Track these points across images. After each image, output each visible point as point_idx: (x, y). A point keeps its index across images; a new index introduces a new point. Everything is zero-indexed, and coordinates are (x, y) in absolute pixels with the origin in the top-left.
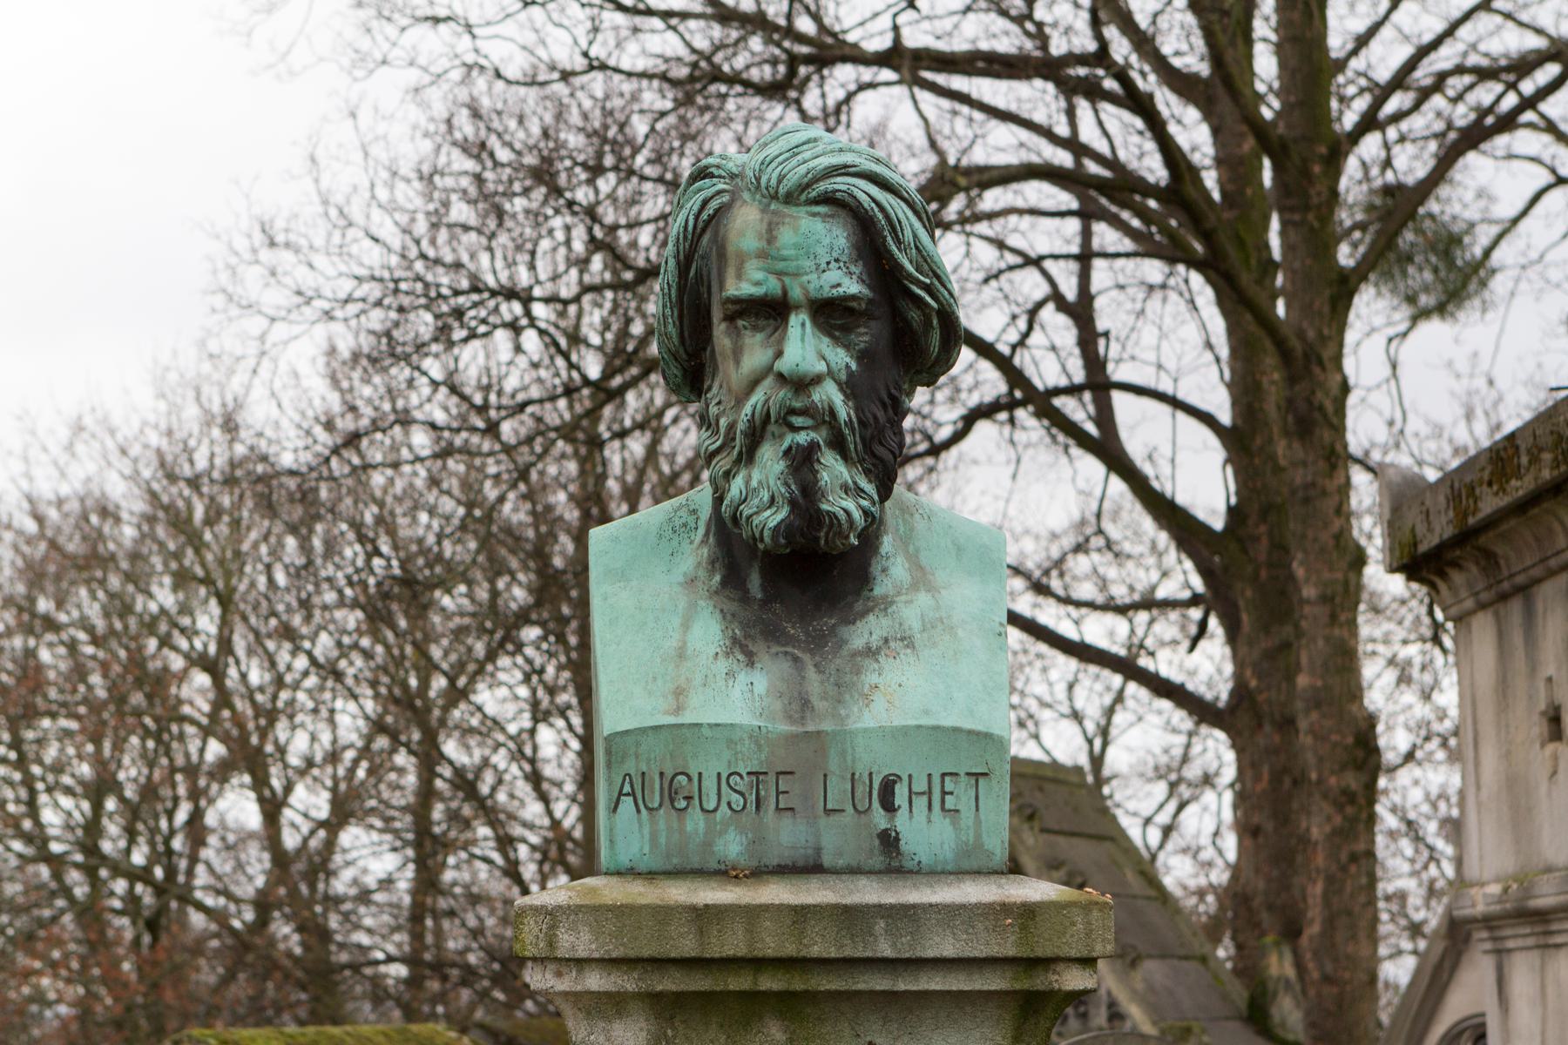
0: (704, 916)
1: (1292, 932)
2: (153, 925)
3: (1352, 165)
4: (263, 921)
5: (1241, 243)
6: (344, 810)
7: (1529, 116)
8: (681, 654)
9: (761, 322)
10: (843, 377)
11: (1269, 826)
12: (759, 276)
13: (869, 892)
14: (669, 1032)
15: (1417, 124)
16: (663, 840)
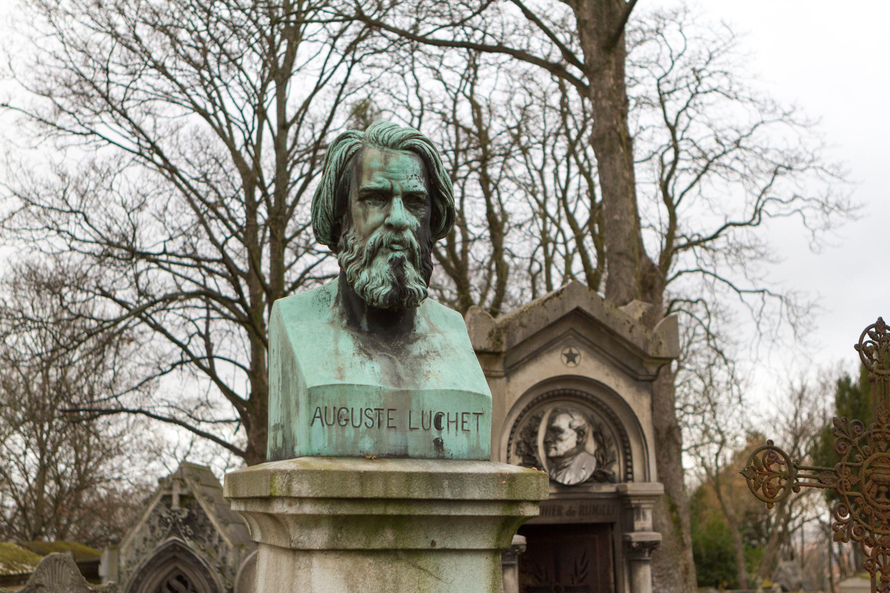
0: (364, 477)
9: (378, 202)
10: (415, 229)
12: (381, 179)
13: (437, 467)
14: (339, 535)
16: (334, 440)
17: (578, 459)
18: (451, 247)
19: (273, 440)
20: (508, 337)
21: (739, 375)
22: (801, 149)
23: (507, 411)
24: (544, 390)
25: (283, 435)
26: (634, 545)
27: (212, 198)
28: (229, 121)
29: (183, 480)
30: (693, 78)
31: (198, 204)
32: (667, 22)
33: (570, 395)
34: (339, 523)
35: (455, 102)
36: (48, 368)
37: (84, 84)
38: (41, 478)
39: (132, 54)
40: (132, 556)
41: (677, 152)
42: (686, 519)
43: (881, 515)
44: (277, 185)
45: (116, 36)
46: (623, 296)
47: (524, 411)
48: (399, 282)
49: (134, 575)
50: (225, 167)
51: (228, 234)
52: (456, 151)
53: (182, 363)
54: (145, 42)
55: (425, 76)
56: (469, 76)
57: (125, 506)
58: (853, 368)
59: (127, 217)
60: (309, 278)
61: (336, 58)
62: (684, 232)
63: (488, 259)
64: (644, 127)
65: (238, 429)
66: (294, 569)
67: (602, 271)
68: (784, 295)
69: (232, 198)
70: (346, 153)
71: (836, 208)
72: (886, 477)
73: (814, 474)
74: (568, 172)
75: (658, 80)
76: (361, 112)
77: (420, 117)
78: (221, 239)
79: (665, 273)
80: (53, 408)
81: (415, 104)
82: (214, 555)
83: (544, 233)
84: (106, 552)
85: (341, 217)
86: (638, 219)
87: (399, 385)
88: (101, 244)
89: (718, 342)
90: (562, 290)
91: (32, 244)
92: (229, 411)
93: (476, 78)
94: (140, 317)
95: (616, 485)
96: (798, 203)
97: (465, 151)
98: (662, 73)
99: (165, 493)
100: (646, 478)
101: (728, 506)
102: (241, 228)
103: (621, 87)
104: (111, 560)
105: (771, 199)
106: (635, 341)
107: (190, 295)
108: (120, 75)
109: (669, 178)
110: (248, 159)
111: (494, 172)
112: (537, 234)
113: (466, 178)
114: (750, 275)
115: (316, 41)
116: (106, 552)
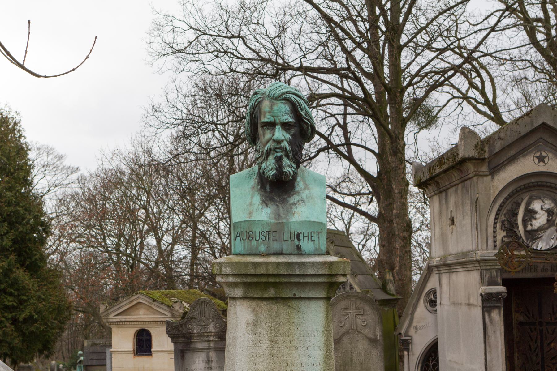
0: (256, 264)
1: (392, 269)
2: (132, 267)
3: (406, 94)
4: (157, 266)
5: (381, 111)
6: (175, 241)
7: (447, 82)
8: (251, 204)
10: (288, 140)
11: (387, 245)
12: (269, 117)
13: (294, 259)
15: (421, 84)
17: (548, 232)
20: (489, 148)
23: (492, 199)
24: (521, 183)
33: (542, 186)
34: (247, 285)
47: (507, 199)
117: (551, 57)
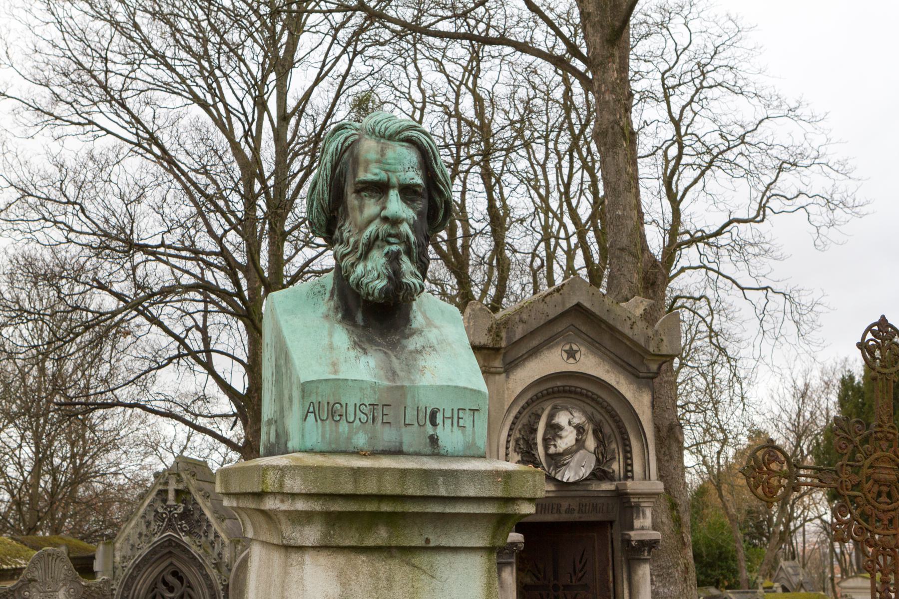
0: (357, 472)
9: (374, 194)
10: (412, 222)
12: (377, 171)
14: (332, 532)
16: (328, 436)
17: (577, 456)
18: (452, 241)
19: (266, 435)
20: (507, 333)
21: (742, 374)
22: (806, 145)
23: (506, 407)
24: (543, 387)
25: (276, 431)
26: (633, 543)
27: (211, 191)
28: (228, 111)
29: (179, 475)
30: (698, 73)
31: (197, 196)
32: (672, 15)
34: (332, 519)
35: (458, 95)
36: (43, 361)
37: (82, 73)
38: (36, 473)
39: (132, 44)
40: (127, 551)
41: (681, 148)
42: (686, 518)
43: (882, 516)
44: (276, 178)
45: (115, 24)
46: (625, 292)
47: (523, 408)
48: (395, 276)
49: (128, 571)
50: (225, 160)
51: (227, 227)
52: (458, 145)
53: (179, 356)
54: (144, 29)
55: (427, 68)
56: (472, 68)
57: (121, 501)
58: (857, 367)
59: (125, 208)
60: (309, 272)
61: (337, 50)
62: (688, 228)
63: (489, 254)
64: (649, 122)
65: (235, 423)
66: (286, 567)
67: (604, 268)
68: (787, 292)
69: (232, 189)
70: (342, 145)
71: (841, 205)
72: (887, 476)
73: (816, 473)
74: (571, 167)
75: (663, 74)
76: (362, 105)
77: (422, 110)
78: (220, 232)
79: (668, 270)
80: (49, 402)
81: (417, 96)
82: (210, 550)
83: (546, 227)
84: (101, 547)
85: (337, 210)
86: (641, 215)
87: (394, 380)
88: (99, 236)
89: (721, 340)
90: (563, 285)
91: (29, 236)
92: (225, 405)
93: (479, 70)
94: (137, 310)
95: (615, 483)
96: (803, 200)
97: (467, 145)
98: (667, 67)
99: (161, 487)
100: (646, 476)
101: (729, 505)
102: (240, 221)
103: (625, 82)
104: (105, 552)
105: (776, 195)
106: (636, 338)
107: (189, 288)
108: (119, 65)
109: (673, 173)
110: (248, 152)
111: (496, 166)
112: (539, 229)
113: (467, 172)
114: (754, 272)
115: (318, 32)
116: (101, 547)
117: (453, 264)
